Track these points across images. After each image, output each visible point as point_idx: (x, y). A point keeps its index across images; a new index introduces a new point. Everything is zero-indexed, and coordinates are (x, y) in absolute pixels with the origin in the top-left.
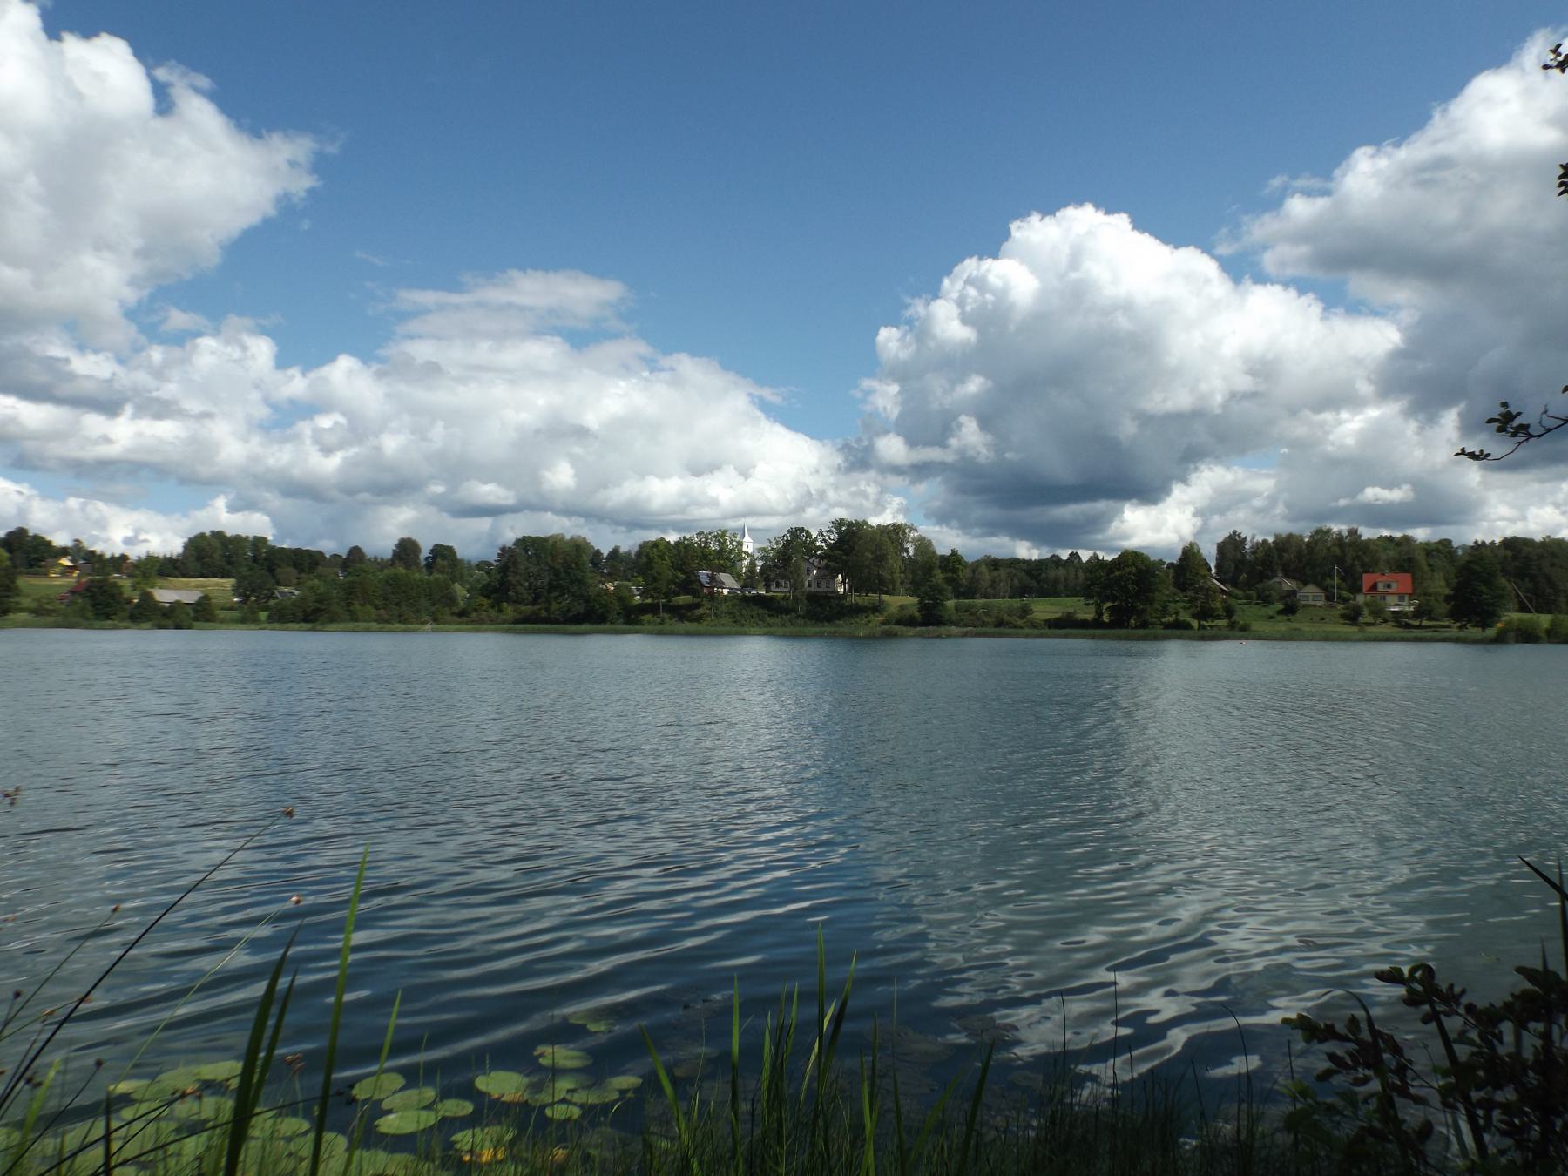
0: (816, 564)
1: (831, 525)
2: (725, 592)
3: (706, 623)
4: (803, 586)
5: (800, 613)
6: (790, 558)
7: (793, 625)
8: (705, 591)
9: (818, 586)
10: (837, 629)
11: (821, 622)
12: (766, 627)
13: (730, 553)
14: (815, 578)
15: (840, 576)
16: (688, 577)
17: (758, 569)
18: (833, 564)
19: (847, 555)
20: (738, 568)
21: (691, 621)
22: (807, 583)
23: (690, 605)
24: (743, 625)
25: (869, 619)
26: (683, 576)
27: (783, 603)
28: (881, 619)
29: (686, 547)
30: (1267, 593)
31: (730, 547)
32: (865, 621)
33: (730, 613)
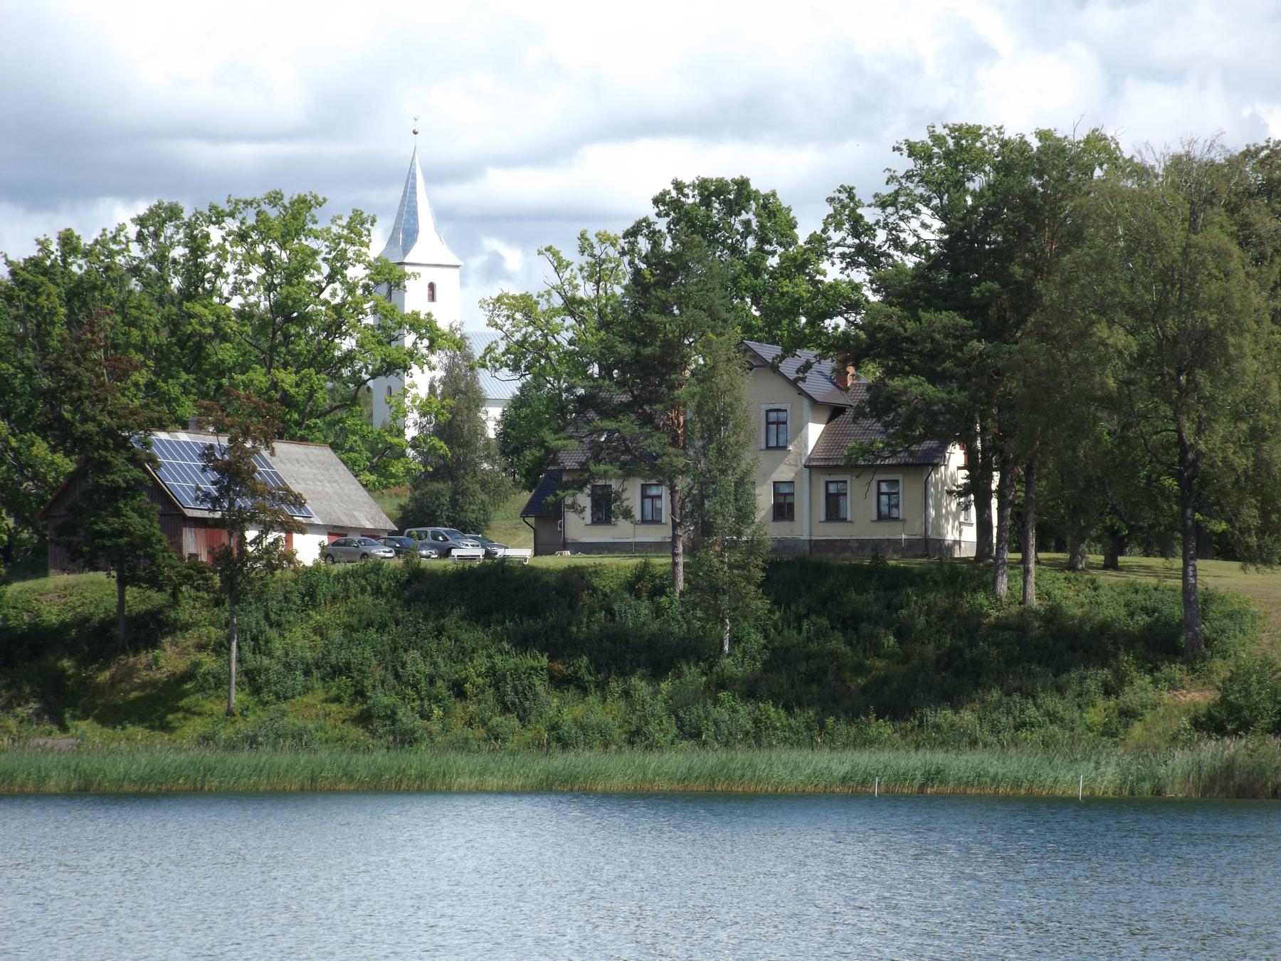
0: (817, 385)
1: (905, 164)
2: (307, 548)
3: (195, 727)
4: (744, 515)
5: (727, 665)
6: (671, 359)
7: (694, 735)
8: (193, 544)
9: (834, 511)
10: (939, 758)
11: (853, 714)
12: (538, 745)
13: (335, 328)
14: (813, 468)
15: (956, 456)
16: (93, 465)
17: (491, 419)
18: (915, 387)
19: (996, 332)
20: (381, 414)
21: (113, 716)
22: (764, 500)
23: (106, 626)
24: (406, 739)
25: (1130, 697)
26: (68, 465)
27: (637, 613)
28: (1199, 697)
29: (78, 293)
30: (946, 568)
31: (334, 294)
32: (1096, 715)
33: (337, 671)
